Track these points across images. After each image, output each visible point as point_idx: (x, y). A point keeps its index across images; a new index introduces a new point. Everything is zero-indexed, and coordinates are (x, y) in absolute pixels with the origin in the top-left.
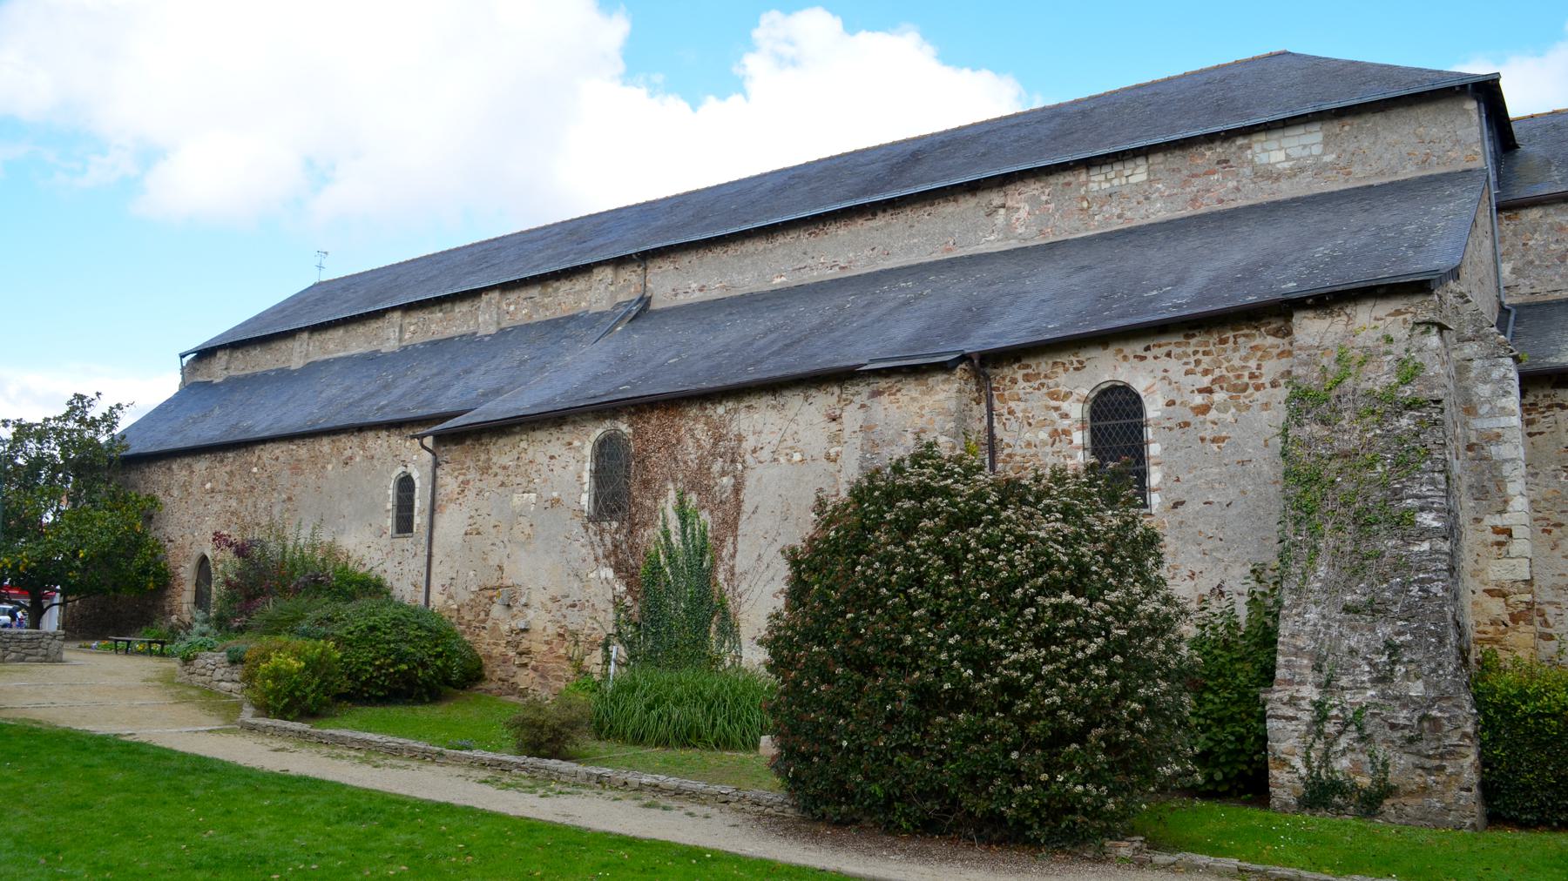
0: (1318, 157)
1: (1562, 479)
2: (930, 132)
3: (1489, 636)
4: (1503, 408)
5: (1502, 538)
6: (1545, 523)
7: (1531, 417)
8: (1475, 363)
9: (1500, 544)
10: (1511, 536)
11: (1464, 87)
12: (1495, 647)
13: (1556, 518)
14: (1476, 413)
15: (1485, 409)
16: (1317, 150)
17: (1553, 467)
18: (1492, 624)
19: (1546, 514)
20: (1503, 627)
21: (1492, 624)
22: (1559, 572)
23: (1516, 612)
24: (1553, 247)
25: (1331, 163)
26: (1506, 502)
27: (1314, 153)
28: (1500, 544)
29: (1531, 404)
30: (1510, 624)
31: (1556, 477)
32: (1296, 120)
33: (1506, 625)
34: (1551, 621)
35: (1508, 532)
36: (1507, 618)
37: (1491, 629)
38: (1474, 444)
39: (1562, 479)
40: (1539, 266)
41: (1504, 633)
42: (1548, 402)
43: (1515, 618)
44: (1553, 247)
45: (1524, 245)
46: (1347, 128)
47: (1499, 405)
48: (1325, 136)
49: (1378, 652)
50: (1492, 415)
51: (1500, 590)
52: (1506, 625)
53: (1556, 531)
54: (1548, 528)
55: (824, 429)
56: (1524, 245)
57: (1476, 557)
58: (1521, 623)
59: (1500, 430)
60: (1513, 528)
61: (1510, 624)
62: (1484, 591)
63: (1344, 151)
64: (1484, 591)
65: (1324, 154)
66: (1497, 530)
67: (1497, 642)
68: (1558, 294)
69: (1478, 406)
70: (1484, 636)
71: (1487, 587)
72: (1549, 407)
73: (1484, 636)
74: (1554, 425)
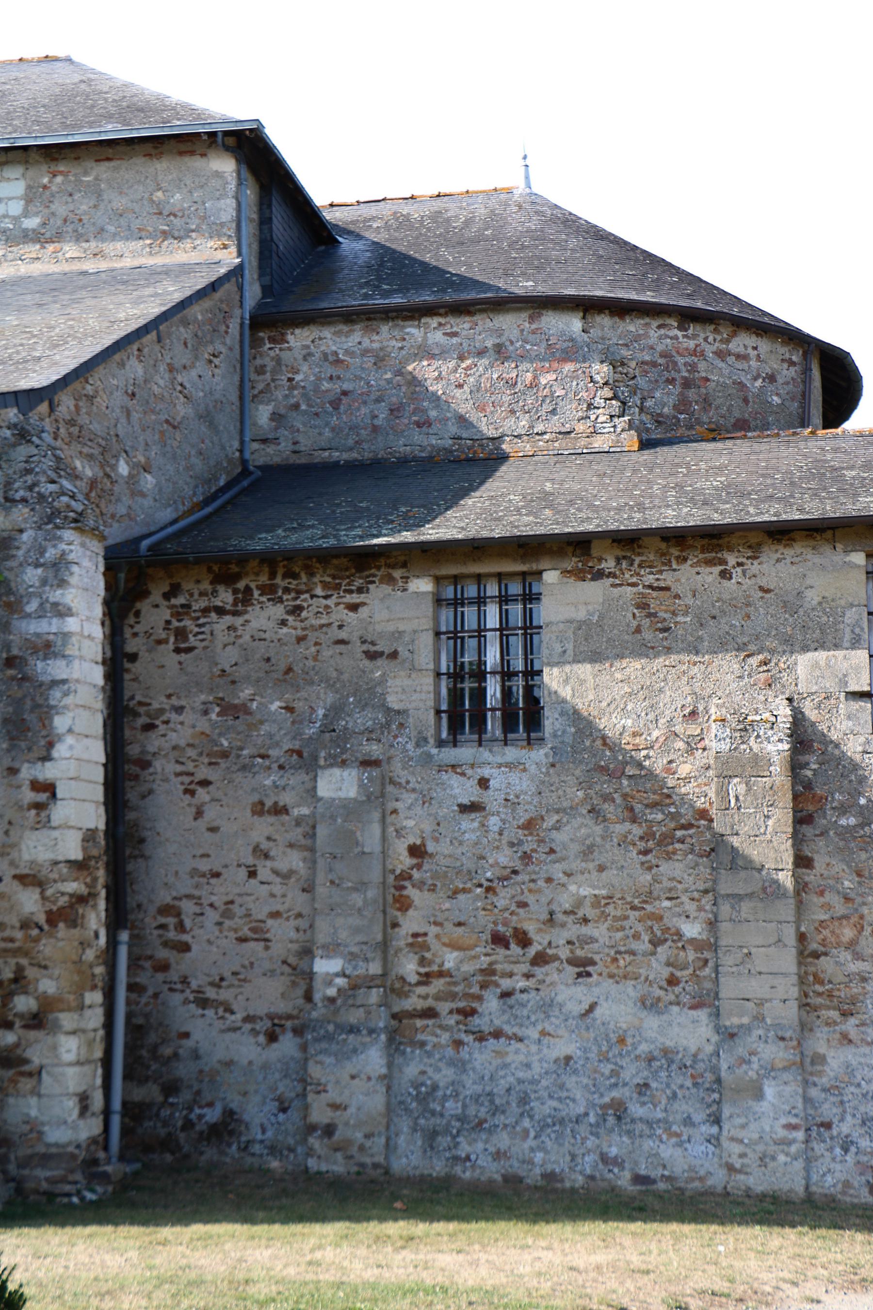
0: (16, 219)
1: (214, 716)
2: (487, 185)
3: (17, 944)
4: (56, 605)
5: (43, 797)
6: (187, 779)
7: (182, 624)
8: (25, 537)
9: (39, 806)
10: (54, 795)
11: (212, 135)
12: (24, 962)
13: (203, 772)
14: (22, 611)
15: (32, 607)
16: (16, 208)
17: (203, 697)
18: (22, 928)
19: (190, 767)
20: (35, 932)
21: (22, 928)
22: (201, 852)
23: (55, 908)
24: (326, 385)
25: (34, 230)
26: (51, 745)
27: (11, 213)
28: (39, 806)
29: (183, 606)
30: (46, 927)
31: (206, 713)
32: (11, 155)
33: (41, 929)
34: (188, 923)
35: (50, 789)
36: (41, 919)
37: (19, 935)
38: (16, 657)
39: (214, 716)
40: (305, 412)
41: (37, 940)
42: (203, 603)
43: (53, 918)
44: (326, 385)
45: (290, 380)
46: (59, 179)
47: (52, 600)
48: (29, 188)
49: (409, 991)
50: (40, 614)
51: (34, 876)
52: (41, 929)
53: (201, 791)
54: (192, 787)
55: (425, 688)
56: (290, 380)
57: (7, 827)
58: (61, 925)
59: (51, 637)
60: (58, 784)
61: (46, 927)
62: (15, 877)
63: (53, 214)
64: (15, 877)
65: (26, 214)
66: (37, 786)
67: (26, 954)
68: (327, 454)
69: (25, 600)
70: (10, 945)
71: (18, 872)
72: (206, 611)
73: (10, 945)
74: (209, 637)
